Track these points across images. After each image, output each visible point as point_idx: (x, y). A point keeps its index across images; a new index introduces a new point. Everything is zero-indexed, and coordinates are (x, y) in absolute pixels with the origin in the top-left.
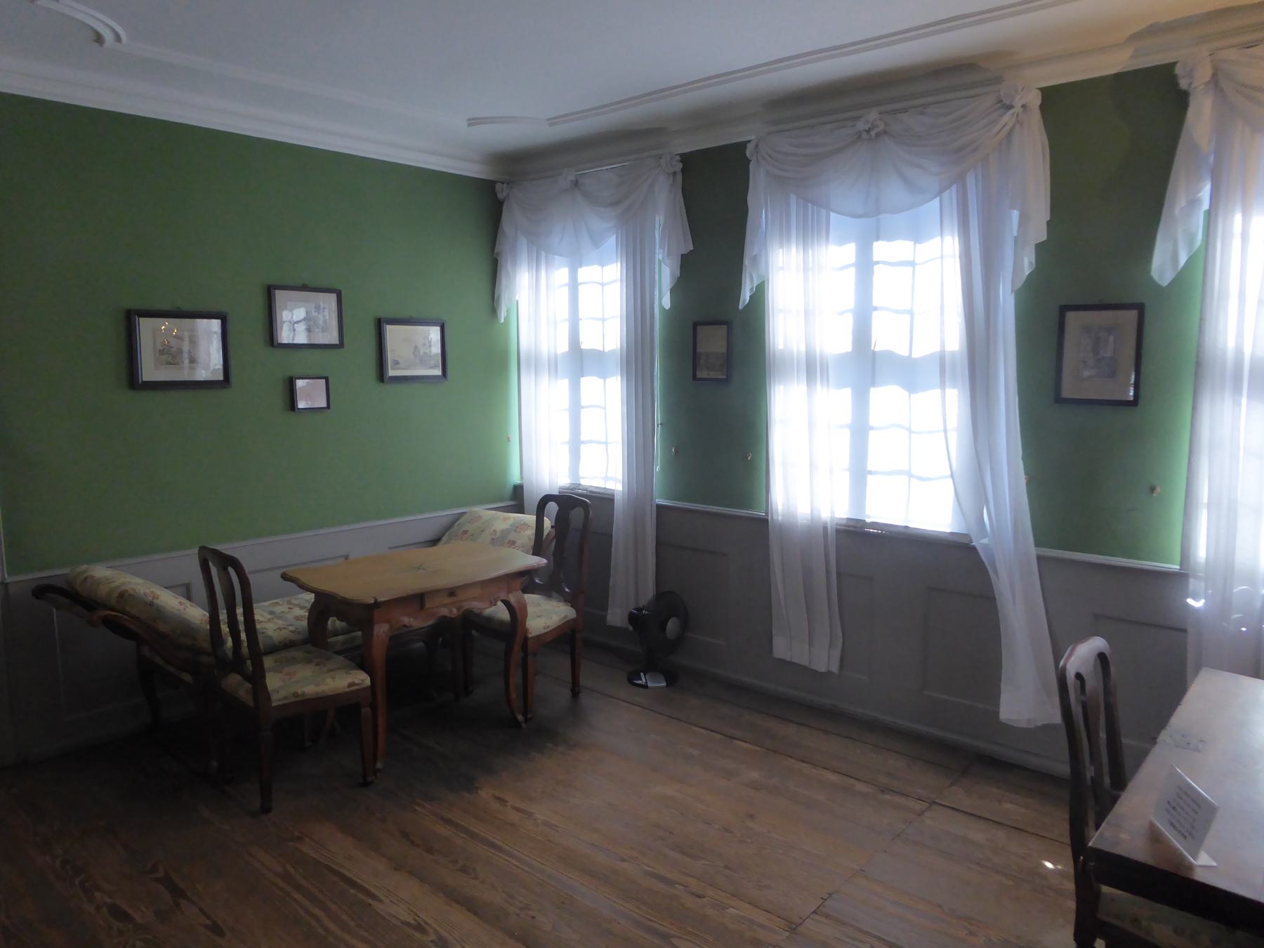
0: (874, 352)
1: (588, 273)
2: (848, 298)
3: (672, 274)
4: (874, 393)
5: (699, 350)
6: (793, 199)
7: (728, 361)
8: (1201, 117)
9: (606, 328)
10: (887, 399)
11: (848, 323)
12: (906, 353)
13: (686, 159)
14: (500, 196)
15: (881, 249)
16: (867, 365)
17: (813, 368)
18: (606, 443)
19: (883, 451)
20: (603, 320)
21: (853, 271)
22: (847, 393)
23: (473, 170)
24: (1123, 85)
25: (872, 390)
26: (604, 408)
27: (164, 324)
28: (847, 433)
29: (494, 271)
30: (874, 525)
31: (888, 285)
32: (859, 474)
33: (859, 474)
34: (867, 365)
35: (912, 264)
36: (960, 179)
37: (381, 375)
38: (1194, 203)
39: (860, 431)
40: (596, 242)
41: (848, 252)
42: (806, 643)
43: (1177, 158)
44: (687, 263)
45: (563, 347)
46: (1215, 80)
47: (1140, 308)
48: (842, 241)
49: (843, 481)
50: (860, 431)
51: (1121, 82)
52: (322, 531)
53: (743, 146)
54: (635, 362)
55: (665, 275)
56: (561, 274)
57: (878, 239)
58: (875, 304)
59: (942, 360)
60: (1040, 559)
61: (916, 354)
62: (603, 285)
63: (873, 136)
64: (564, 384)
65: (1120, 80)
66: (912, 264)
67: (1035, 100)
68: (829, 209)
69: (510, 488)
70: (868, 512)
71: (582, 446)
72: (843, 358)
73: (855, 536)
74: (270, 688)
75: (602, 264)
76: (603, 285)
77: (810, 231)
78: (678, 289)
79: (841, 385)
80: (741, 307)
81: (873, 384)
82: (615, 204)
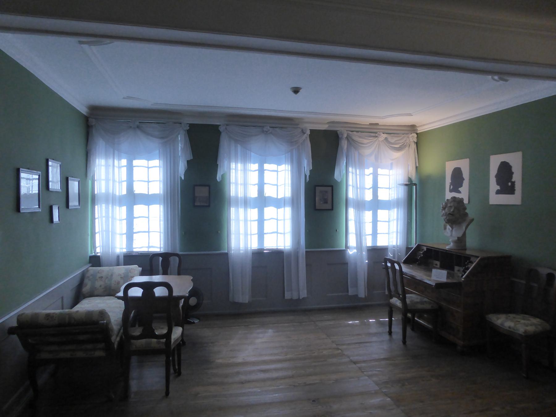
0: (265, 197)
5: (196, 195)
8: (344, 144)
10: (139, 209)
13: (192, 126)
16: (262, 201)
17: (246, 203)
18: (149, 232)
19: (268, 227)
20: (148, 182)
22: (256, 210)
23: (84, 110)
24: (325, 133)
25: (265, 209)
26: (148, 217)
27: (317, 204)
29: (87, 157)
31: (269, 177)
32: (261, 234)
33: (261, 234)
35: (277, 171)
37: (18, 209)
42: (242, 294)
46: (347, 138)
47: (332, 186)
50: (261, 221)
52: (231, 284)
55: (182, 167)
56: (124, 162)
58: (265, 182)
60: (306, 252)
61: (279, 197)
63: (266, 133)
65: (325, 131)
66: (277, 171)
67: (308, 132)
70: (265, 246)
73: (259, 255)
77: (245, 159)
82: (162, 138)
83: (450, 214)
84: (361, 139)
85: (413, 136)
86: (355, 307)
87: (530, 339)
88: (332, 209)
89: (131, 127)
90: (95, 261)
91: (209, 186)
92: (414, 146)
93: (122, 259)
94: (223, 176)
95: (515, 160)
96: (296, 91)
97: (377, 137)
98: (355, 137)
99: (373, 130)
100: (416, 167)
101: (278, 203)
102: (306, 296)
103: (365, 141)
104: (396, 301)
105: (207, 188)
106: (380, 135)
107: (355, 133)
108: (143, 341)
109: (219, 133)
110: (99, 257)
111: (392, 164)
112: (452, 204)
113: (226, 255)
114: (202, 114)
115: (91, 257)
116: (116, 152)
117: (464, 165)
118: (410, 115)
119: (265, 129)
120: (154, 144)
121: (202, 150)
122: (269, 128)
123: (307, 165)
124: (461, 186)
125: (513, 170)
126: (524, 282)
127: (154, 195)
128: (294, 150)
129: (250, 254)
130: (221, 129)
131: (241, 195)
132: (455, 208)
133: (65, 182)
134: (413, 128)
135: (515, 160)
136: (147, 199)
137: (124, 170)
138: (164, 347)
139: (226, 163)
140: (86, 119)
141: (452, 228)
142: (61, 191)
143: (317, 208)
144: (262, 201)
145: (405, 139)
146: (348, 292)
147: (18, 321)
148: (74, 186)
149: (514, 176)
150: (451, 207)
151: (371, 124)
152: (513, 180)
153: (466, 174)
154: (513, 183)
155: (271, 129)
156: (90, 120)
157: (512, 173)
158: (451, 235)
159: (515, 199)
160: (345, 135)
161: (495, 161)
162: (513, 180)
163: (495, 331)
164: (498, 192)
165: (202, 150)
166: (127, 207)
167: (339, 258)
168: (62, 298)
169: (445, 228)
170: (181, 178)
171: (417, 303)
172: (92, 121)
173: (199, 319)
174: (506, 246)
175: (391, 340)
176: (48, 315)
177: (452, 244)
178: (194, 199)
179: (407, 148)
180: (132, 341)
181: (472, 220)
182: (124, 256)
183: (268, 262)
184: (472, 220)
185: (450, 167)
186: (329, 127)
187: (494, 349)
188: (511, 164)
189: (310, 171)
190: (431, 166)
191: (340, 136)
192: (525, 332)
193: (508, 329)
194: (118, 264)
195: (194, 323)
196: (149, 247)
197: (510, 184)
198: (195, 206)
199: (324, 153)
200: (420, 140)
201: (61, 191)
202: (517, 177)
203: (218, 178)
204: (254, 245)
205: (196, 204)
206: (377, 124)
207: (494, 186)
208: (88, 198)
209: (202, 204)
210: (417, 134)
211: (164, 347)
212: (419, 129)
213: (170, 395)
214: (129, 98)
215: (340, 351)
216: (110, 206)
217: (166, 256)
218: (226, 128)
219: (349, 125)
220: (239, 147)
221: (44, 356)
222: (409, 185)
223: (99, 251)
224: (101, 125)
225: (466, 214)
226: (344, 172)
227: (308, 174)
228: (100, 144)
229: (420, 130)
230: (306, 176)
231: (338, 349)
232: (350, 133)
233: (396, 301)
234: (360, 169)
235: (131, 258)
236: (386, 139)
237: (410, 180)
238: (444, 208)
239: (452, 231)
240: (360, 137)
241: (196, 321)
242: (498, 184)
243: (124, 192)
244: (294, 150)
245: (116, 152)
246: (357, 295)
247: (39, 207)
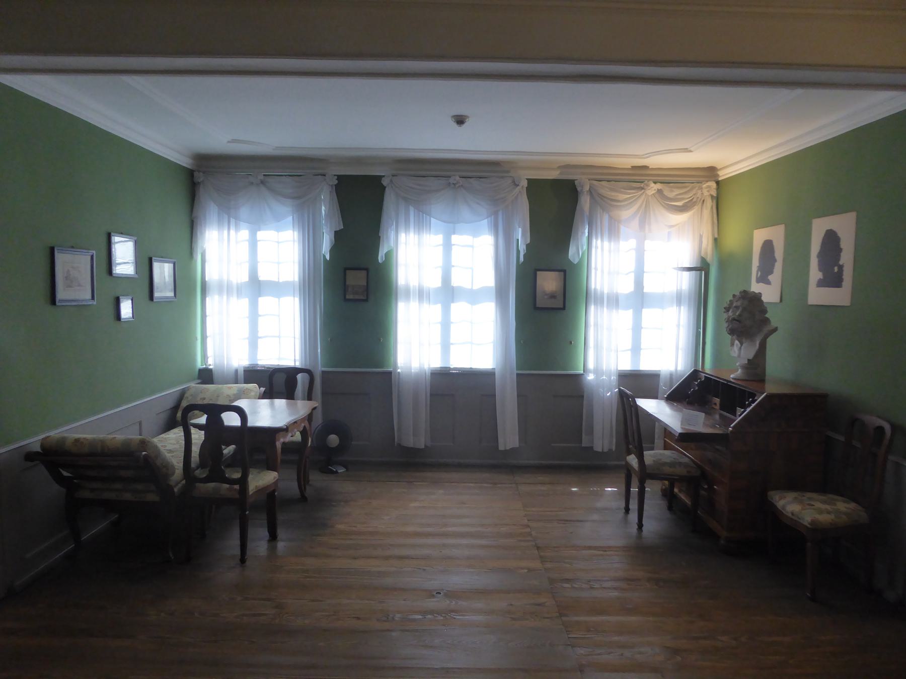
1: (266, 236)
2: (439, 260)
3: (331, 240)
4: (453, 306)
6: (412, 209)
7: (367, 290)
8: (585, 202)
9: (487, 277)
10: (266, 303)
11: (631, 278)
12: (469, 287)
13: (340, 178)
14: (196, 180)
15: (455, 238)
16: (256, 287)
18: (279, 337)
20: (279, 263)
21: (441, 248)
22: (630, 312)
23: (185, 161)
24: (556, 184)
25: (452, 305)
28: (439, 326)
29: (192, 228)
30: (455, 369)
32: (446, 346)
33: (446, 346)
34: (256, 287)
35: (472, 246)
36: (496, 214)
38: (583, 233)
39: (446, 325)
40: (278, 218)
41: (439, 239)
43: (385, 203)
44: (338, 235)
45: (245, 278)
47: (564, 271)
48: (436, 233)
49: (245, 346)
50: (446, 325)
51: (555, 183)
53: (378, 178)
54: (307, 287)
57: (454, 233)
59: (484, 290)
60: (517, 374)
61: (475, 288)
62: (278, 242)
63: (454, 186)
64: (245, 302)
66: (472, 246)
67: (525, 183)
68: (430, 216)
69: (197, 371)
71: (259, 340)
72: (437, 290)
74: (779, 507)
75: (278, 230)
76: (278, 242)
77: (421, 226)
78: (333, 250)
79: (436, 303)
80: (380, 261)
81: (260, 296)
82: (299, 198)
83: (734, 319)
84: (613, 194)
85: (709, 187)
86: (589, 466)
87: (825, 536)
88: (564, 308)
89: (252, 183)
90: (206, 376)
91: (367, 269)
92: (709, 203)
93: (241, 373)
94: (388, 255)
95: (845, 225)
96: (460, 121)
97: (642, 188)
98: (604, 189)
99: (637, 178)
100: (716, 240)
101: (474, 296)
102: (517, 445)
103: (622, 197)
104: (633, 460)
105: (364, 273)
106: (648, 186)
107: (603, 183)
108: (212, 485)
109: (384, 188)
110: (211, 370)
111: (669, 233)
112: (739, 303)
113: (576, 379)
114: (359, 161)
115: (201, 371)
116: (233, 221)
117: (776, 234)
118: (686, 150)
119: (451, 180)
120: (285, 209)
121: (356, 213)
122: (458, 178)
123: (521, 236)
124: (771, 272)
125: (843, 245)
126: (842, 438)
127: (287, 284)
128: (500, 213)
129: (428, 373)
130: (385, 182)
131: (414, 283)
132: (744, 309)
133: (145, 264)
134: (711, 172)
135: (845, 225)
136: (277, 288)
137: (245, 247)
138: (237, 496)
139: (392, 234)
140: (190, 173)
141: (742, 344)
142: (136, 276)
143: (539, 305)
144: (448, 293)
145: (694, 191)
146: (581, 442)
147: (42, 446)
148: (163, 271)
149: (842, 254)
150: (737, 307)
151: (634, 168)
152: (841, 263)
153: (779, 253)
154: (841, 268)
155: (462, 181)
156: (196, 174)
157: (840, 250)
158: (739, 356)
159: (840, 296)
160: (587, 188)
161: (819, 228)
162: (841, 263)
163: (774, 515)
164: (821, 284)
165: (356, 213)
166: (248, 301)
167: (572, 388)
168: (140, 423)
169: (732, 345)
170: (324, 256)
171: (665, 464)
172: (199, 177)
173: (345, 467)
174: (828, 378)
175: (625, 520)
176: (77, 441)
177: (740, 371)
178: (345, 288)
179: (696, 209)
180: (198, 485)
181: (775, 330)
182: (390, 373)
183: (453, 388)
184: (775, 330)
185: (760, 236)
186: (561, 174)
187: (768, 547)
188: (840, 234)
189: (527, 246)
190: (733, 240)
191: (579, 189)
192: (813, 522)
193: (790, 515)
194: (236, 382)
195: (336, 472)
196: (279, 359)
197: (836, 269)
198: (346, 300)
199: (554, 216)
200: (715, 192)
201: (136, 276)
202: (847, 258)
203: (381, 258)
204: (435, 362)
205: (348, 297)
206: (645, 167)
207: (815, 274)
208: (188, 286)
209: (357, 297)
210: (718, 183)
211: (237, 496)
212: (720, 173)
213: (248, 563)
214: (234, 141)
215: (528, 530)
216: (225, 297)
217: (290, 373)
218: (391, 181)
219: (600, 171)
220: (412, 209)
221: (86, 494)
222: (702, 268)
223: (211, 363)
224: (205, 183)
225: (766, 321)
226: (585, 247)
227: (522, 248)
228: (210, 210)
229: (723, 175)
230: (518, 252)
231: (528, 526)
232: (595, 183)
233: (633, 460)
234: (610, 241)
235: (253, 374)
236: (660, 191)
237: (703, 260)
238: (727, 310)
239: (740, 348)
240: (612, 190)
241: (341, 470)
242: (820, 270)
243: (246, 278)
244: (500, 213)
245: (233, 221)
246: (592, 447)
247: (93, 298)
